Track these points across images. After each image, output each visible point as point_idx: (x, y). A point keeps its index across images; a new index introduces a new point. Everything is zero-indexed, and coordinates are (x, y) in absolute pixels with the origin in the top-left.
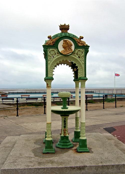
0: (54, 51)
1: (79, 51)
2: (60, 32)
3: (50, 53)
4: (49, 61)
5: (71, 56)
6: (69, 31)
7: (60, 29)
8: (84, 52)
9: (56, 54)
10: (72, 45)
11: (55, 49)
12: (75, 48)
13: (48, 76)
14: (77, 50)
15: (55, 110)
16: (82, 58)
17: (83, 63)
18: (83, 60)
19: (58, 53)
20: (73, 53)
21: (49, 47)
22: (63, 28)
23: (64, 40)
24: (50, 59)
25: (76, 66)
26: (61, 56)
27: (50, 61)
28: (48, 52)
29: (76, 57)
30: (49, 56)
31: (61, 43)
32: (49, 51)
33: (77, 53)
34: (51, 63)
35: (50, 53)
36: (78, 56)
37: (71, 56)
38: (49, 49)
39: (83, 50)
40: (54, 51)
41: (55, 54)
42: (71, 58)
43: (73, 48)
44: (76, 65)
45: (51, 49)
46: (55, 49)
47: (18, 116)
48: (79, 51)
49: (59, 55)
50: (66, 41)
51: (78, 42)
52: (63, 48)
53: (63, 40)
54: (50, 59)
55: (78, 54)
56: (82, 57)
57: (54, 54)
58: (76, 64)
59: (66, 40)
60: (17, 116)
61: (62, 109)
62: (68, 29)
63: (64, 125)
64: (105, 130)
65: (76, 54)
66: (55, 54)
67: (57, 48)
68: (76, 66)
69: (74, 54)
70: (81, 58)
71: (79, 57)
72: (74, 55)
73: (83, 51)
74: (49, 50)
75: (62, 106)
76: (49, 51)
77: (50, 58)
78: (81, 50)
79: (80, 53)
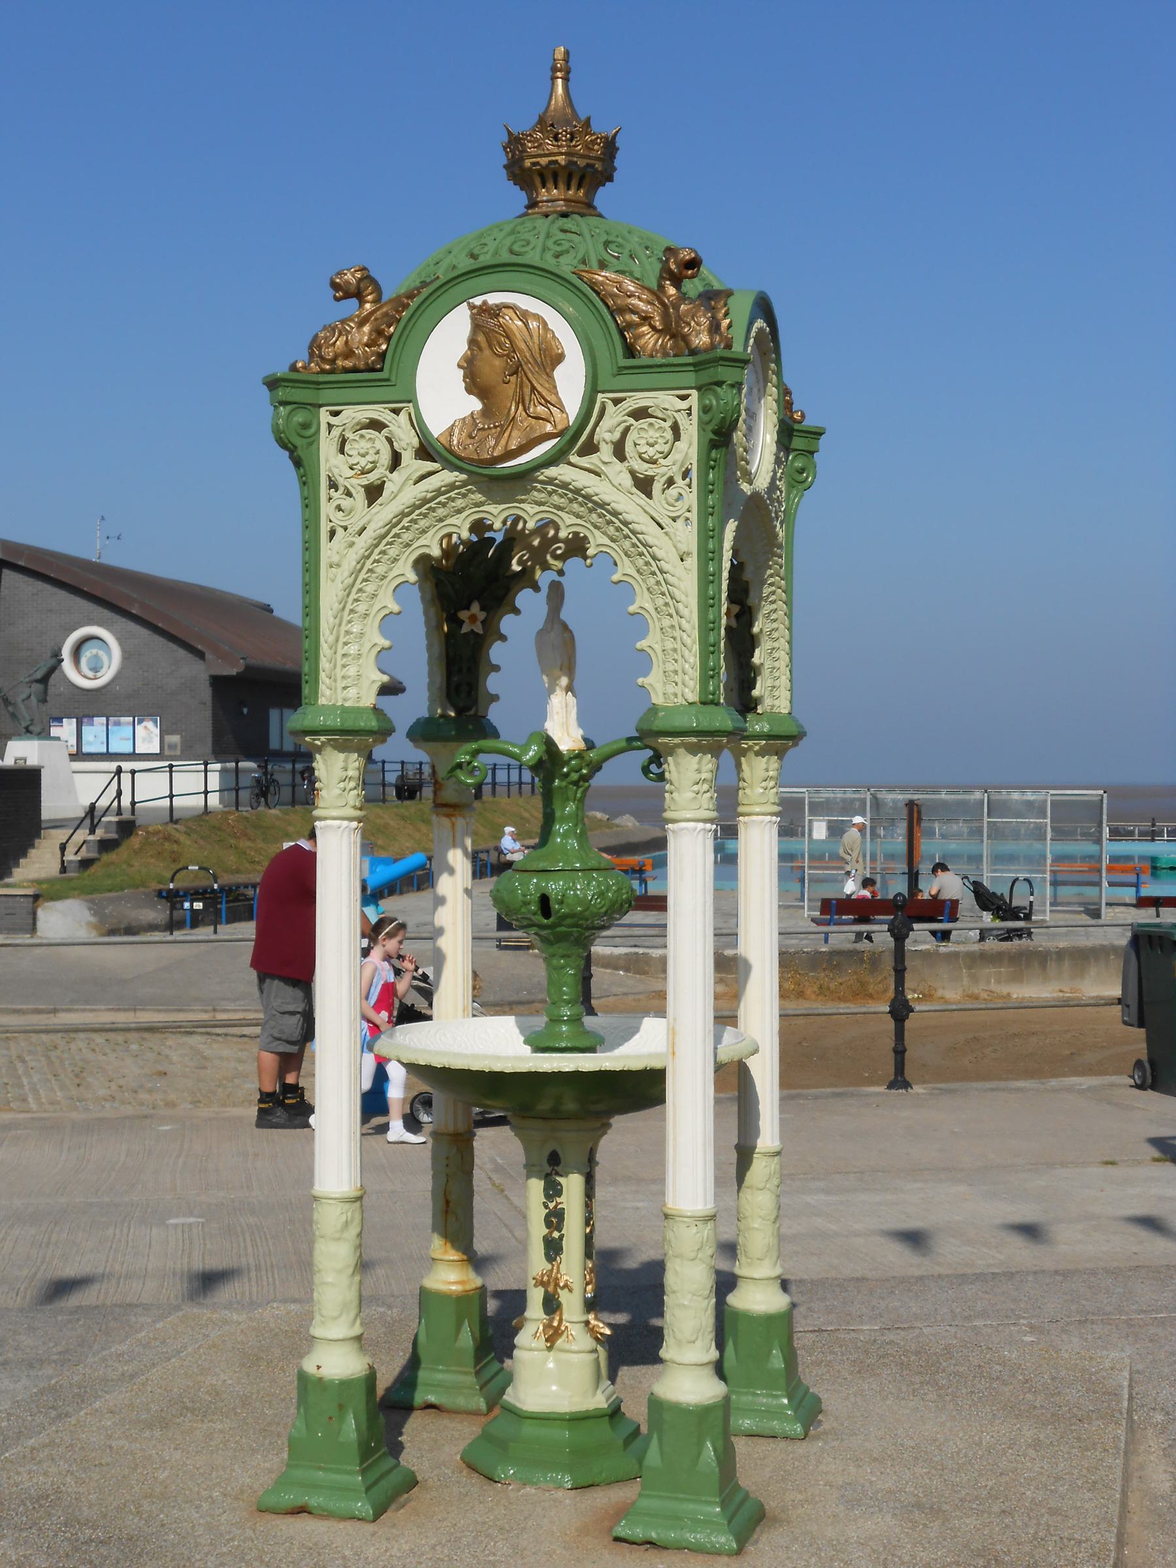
0: (376, 425)
1: (640, 414)
3: (342, 451)
4: (332, 533)
5: (551, 481)
8: (691, 429)
9: (407, 457)
10: (559, 358)
11: (396, 412)
12: (593, 389)
13: (322, 701)
14: (616, 402)
15: (437, 1062)
16: (673, 492)
17: (683, 548)
20: (577, 440)
21: (327, 395)
22: (544, 161)
23: (478, 301)
24: (338, 518)
26: (448, 477)
27: (340, 532)
28: (327, 445)
29: (610, 483)
30: (333, 485)
32: (336, 432)
33: (617, 435)
35: (342, 451)
36: (633, 473)
38: (336, 414)
39: (683, 398)
40: (376, 425)
41: (396, 461)
42: (562, 502)
43: (570, 382)
45: (353, 414)
46: (396, 412)
47: (906, 1085)
48: (640, 414)
50: (494, 312)
51: (633, 311)
52: (469, 391)
53: (472, 307)
56: (670, 482)
59: (494, 299)
60: (891, 1086)
62: (607, 176)
63: (548, 1224)
64: (663, 1293)
65: (606, 452)
66: (396, 461)
69: (581, 454)
70: (657, 487)
71: (644, 485)
72: (584, 461)
74: (330, 426)
76: (336, 432)
78: (665, 400)
79: (652, 434)
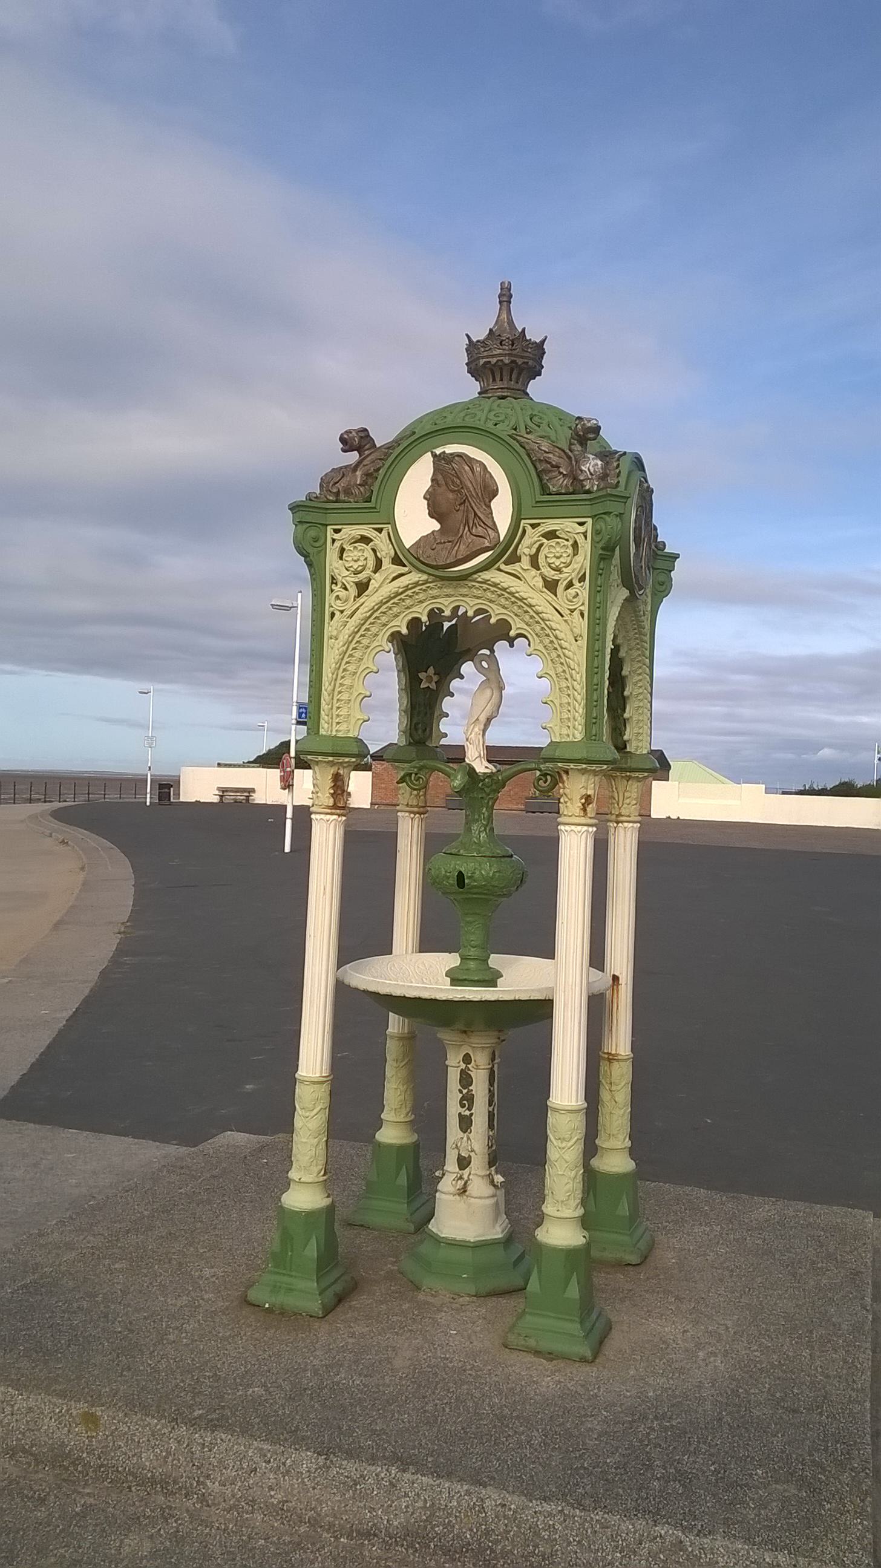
0: (365, 540)
1: (551, 535)
2: (471, 388)
4: (333, 615)
5: (485, 582)
6: (536, 388)
7: (475, 370)
8: (586, 546)
9: (386, 563)
11: (380, 530)
12: (518, 517)
16: (572, 591)
17: (577, 631)
18: (577, 604)
19: (396, 561)
25: (404, 631)
28: (332, 553)
31: (418, 479)
32: (337, 544)
34: (344, 636)
36: (541, 575)
37: (491, 575)
38: (337, 531)
39: (581, 524)
40: (365, 540)
44: (399, 632)
45: (350, 531)
46: (380, 530)
48: (551, 535)
49: (406, 569)
52: (431, 516)
53: (434, 456)
54: (338, 605)
55: (541, 560)
56: (570, 585)
57: (371, 563)
58: (410, 617)
59: (450, 449)
61: (456, 981)
65: (525, 562)
67: (392, 521)
68: (404, 631)
71: (551, 586)
73: (542, 529)
74: (334, 541)
75: (452, 960)
76: (337, 544)
77: (338, 597)
